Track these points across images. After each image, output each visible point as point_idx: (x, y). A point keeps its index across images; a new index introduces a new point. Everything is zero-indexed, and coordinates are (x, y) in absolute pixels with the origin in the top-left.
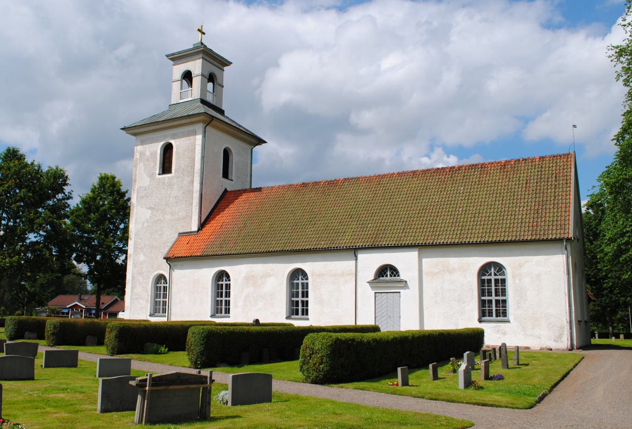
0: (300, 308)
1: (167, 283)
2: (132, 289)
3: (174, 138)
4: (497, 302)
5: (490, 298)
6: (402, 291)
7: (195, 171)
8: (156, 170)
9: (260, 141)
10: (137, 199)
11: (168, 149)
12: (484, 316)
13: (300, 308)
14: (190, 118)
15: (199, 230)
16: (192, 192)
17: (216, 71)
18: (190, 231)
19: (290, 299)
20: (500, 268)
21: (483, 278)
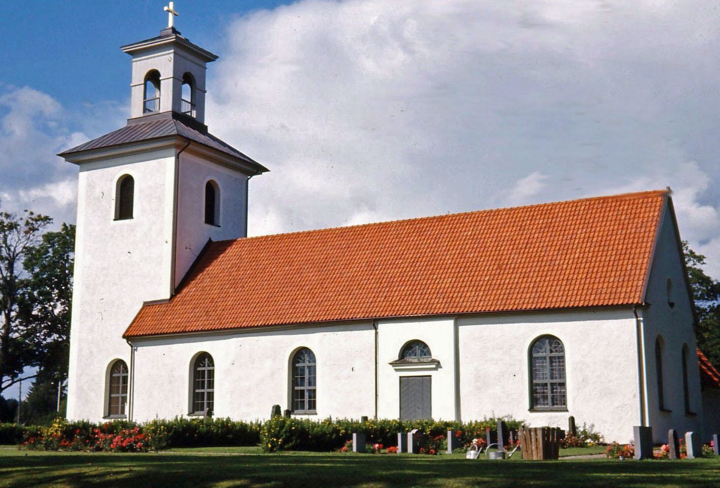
1: (127, 372)
9: (259, 169)
11: (126, 186)
15: (173, 296)
17: (194, 71)
19: (293, 388)
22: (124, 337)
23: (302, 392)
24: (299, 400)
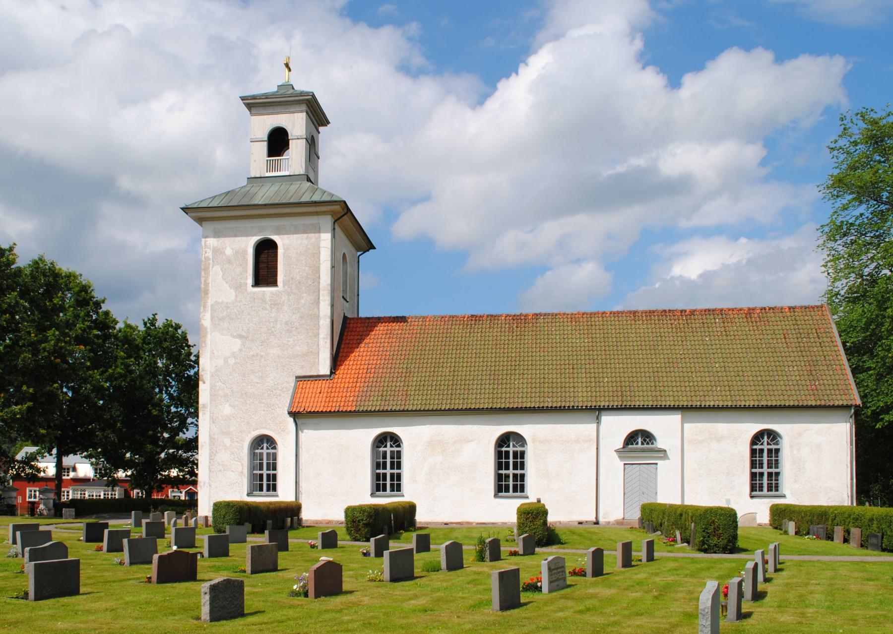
0: (265, 482)
2: (210, 456)
3: (279, 232)
4: (515, 476)
5: (761, 470)
6: (660, 462)
7: (321, 286)
8: (246, 278)
10: (212, 320)
12: (378, 490)
13: (265, 482)
14: (316, 206)
15: (332, 373)
16: (317, 317)
18: (316, 374)
20: (520, 439)
21: (755, 447)
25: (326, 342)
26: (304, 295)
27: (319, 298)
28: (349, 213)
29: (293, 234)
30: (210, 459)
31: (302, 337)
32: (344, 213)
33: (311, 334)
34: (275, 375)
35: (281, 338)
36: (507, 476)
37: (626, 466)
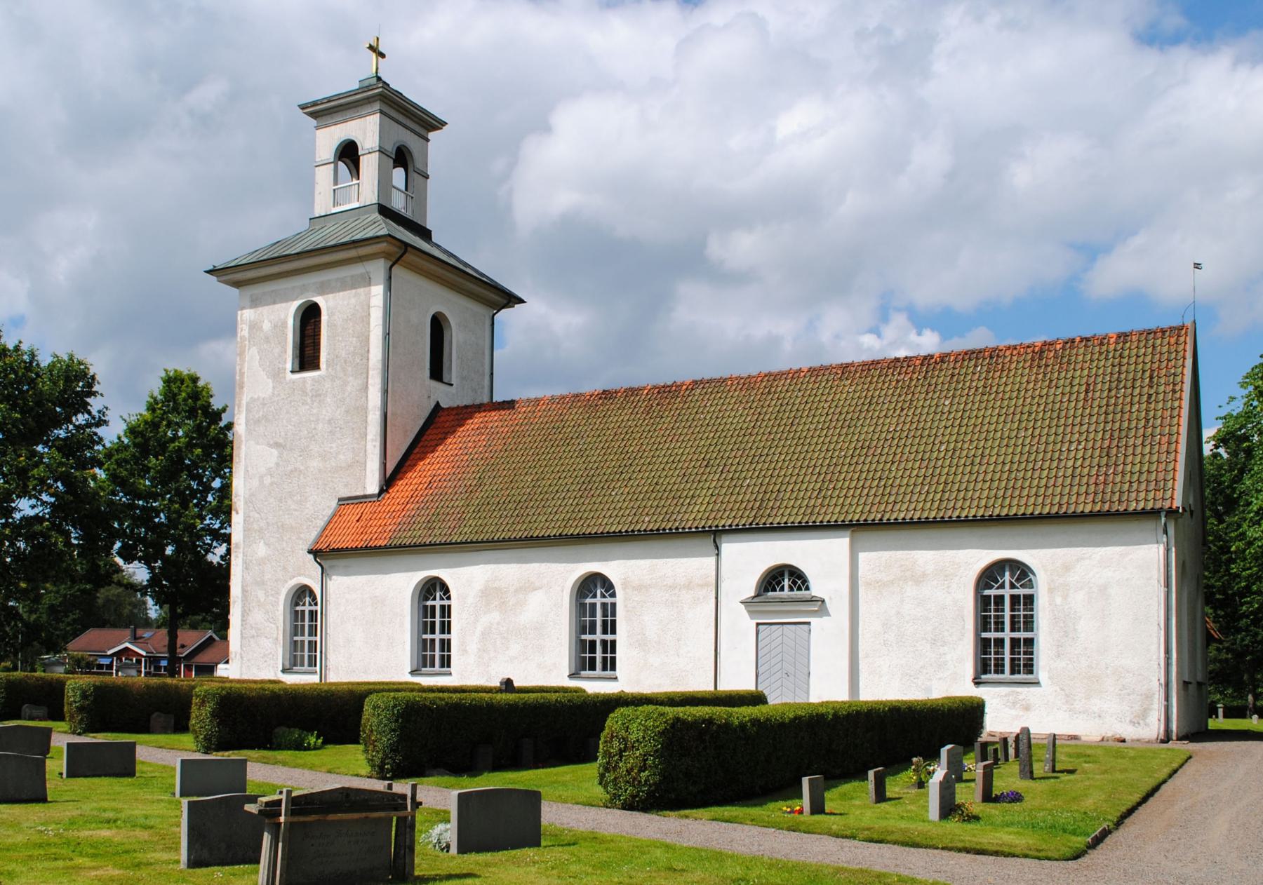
1: (316, 604)
2: (243, 616)
3: (324, 289)
8: (285, 362)
9: (511, 300)
11: (310, 317)
12: (985, 670)
13: (599, 655)
14: (355, 247)
15: (381, 491)
16: (365, 410)
18: (361, 493)
21: (987, 592)
22: (310, 552)
23: (593, 643)
24: (588, 655)
25: (375, 446)
26: (351, 378)
27: (367, 382)
28: (409, 249)
29: (339, 291)
30: (243, 621)
31: (347, 441)
32: (402, 251)
33: (357, 436)
34: (316, 497)
35: (323, 443)
36: (1000, 642)
37: (760, 627)
